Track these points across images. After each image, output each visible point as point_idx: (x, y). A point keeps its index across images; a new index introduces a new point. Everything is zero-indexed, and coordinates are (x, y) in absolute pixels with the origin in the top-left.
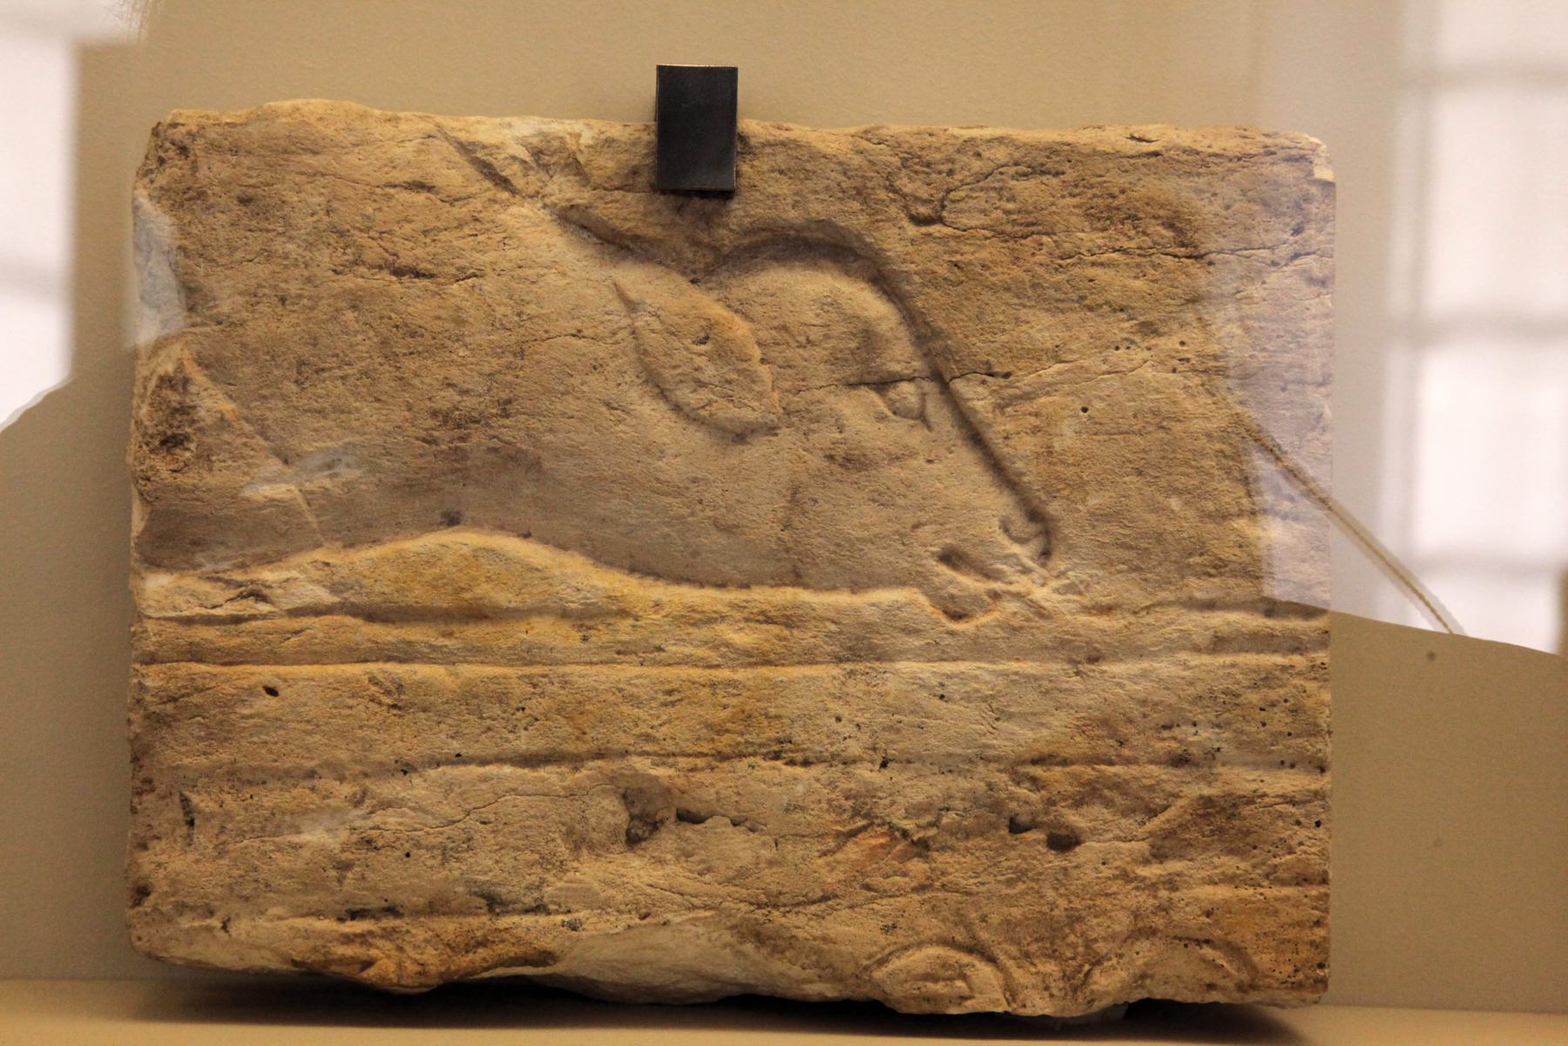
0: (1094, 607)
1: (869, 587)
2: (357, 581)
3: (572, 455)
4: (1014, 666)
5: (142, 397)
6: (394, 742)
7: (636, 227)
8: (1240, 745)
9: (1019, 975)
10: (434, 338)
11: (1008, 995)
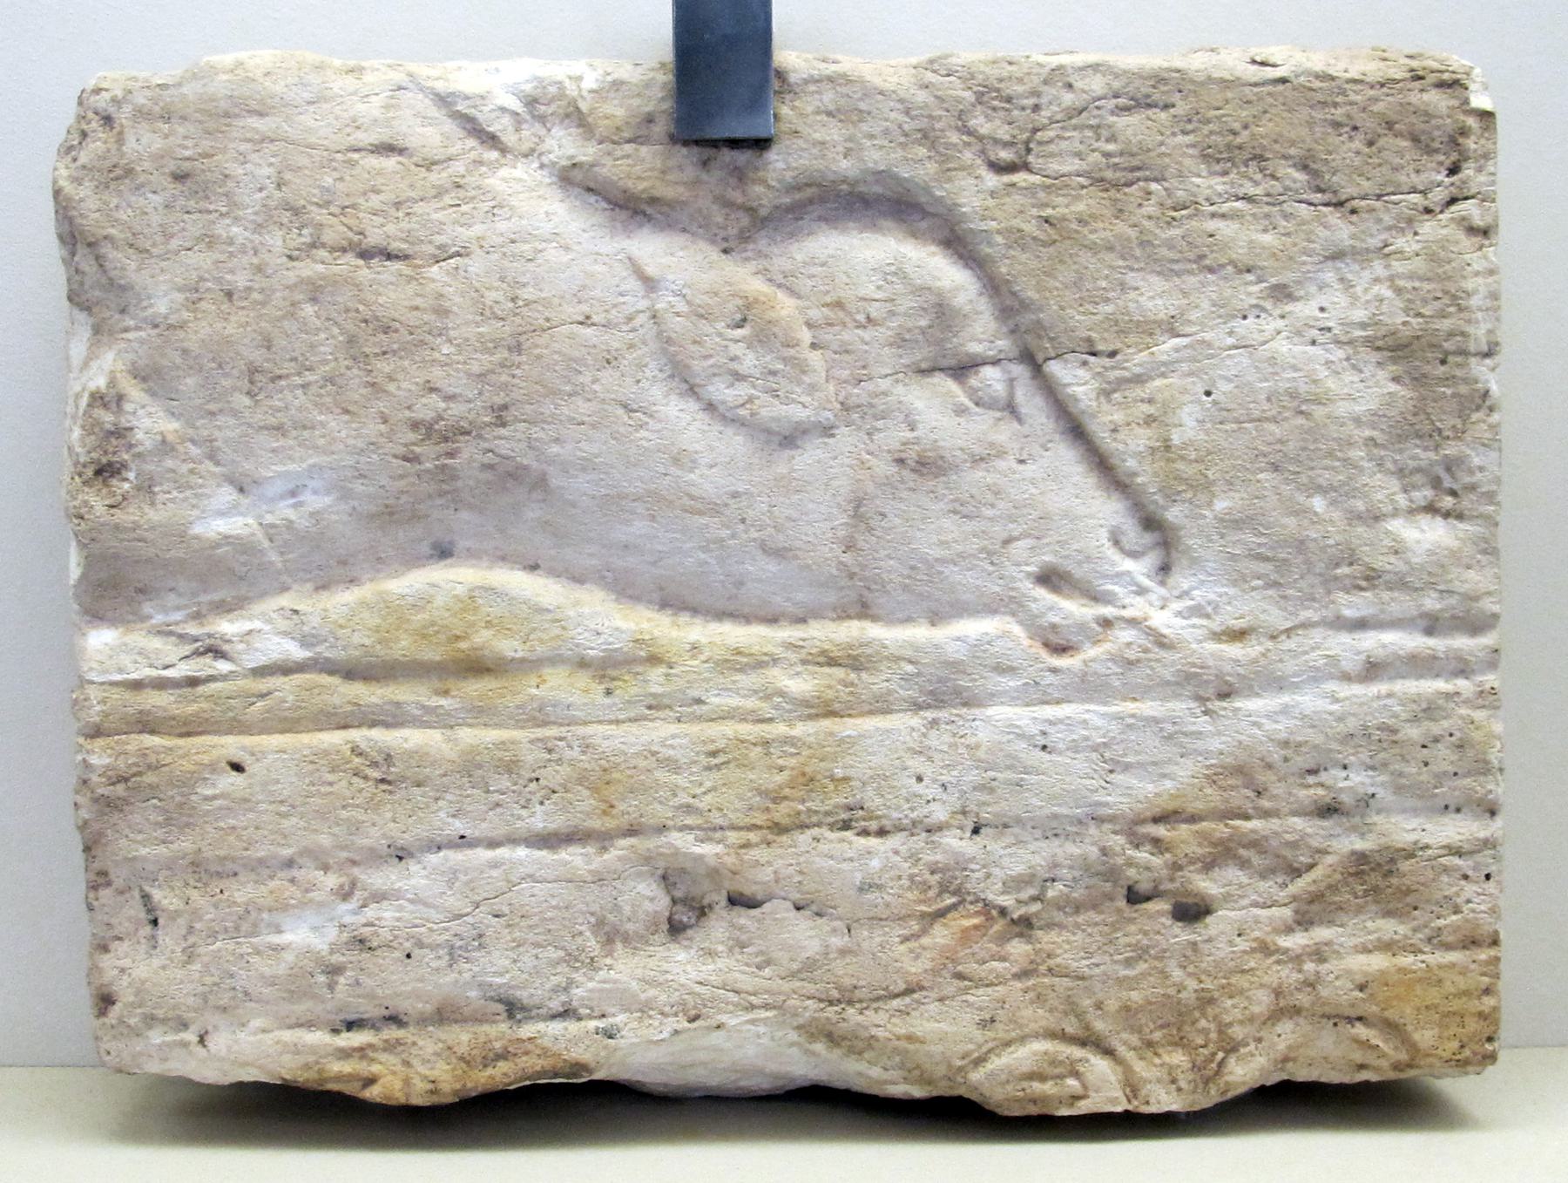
0: (1224, 633)
1: (950, 617)
2: (331, 632)
3: (584, 469)
4: (1130, 707)
5: (74, 417)
6: (382, 828)
7: (653, 187)
8: (1398, 789)
9: (1139, 1067)
10: (412, 334)
11: (1128, 1090)
